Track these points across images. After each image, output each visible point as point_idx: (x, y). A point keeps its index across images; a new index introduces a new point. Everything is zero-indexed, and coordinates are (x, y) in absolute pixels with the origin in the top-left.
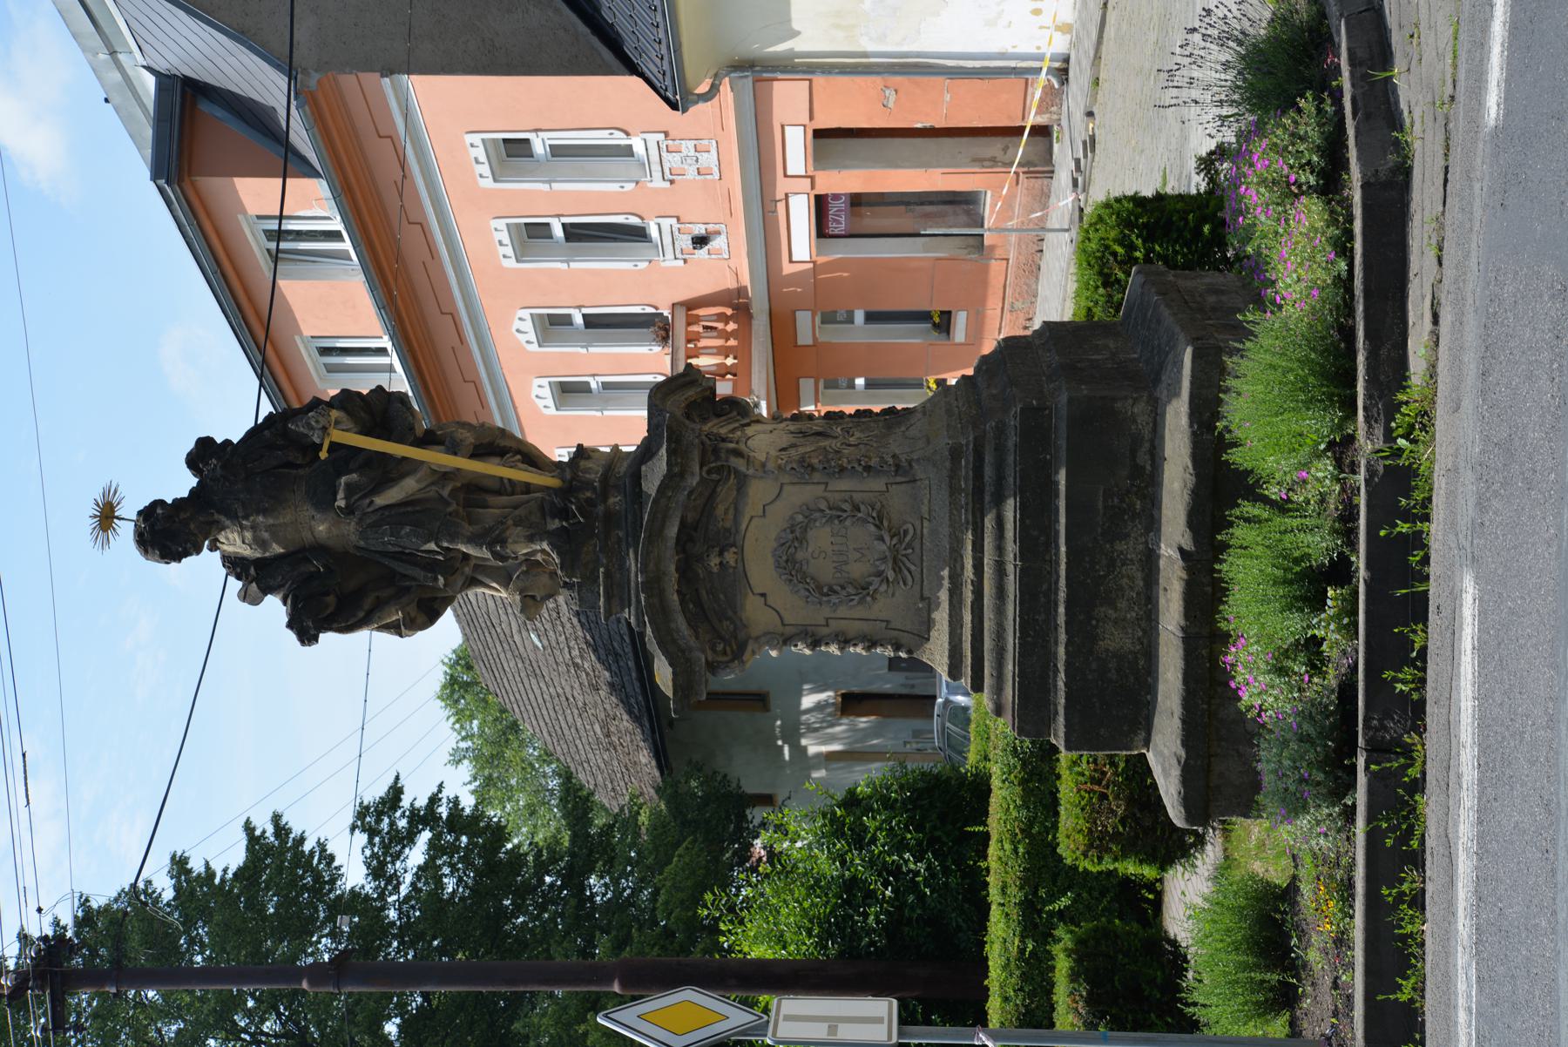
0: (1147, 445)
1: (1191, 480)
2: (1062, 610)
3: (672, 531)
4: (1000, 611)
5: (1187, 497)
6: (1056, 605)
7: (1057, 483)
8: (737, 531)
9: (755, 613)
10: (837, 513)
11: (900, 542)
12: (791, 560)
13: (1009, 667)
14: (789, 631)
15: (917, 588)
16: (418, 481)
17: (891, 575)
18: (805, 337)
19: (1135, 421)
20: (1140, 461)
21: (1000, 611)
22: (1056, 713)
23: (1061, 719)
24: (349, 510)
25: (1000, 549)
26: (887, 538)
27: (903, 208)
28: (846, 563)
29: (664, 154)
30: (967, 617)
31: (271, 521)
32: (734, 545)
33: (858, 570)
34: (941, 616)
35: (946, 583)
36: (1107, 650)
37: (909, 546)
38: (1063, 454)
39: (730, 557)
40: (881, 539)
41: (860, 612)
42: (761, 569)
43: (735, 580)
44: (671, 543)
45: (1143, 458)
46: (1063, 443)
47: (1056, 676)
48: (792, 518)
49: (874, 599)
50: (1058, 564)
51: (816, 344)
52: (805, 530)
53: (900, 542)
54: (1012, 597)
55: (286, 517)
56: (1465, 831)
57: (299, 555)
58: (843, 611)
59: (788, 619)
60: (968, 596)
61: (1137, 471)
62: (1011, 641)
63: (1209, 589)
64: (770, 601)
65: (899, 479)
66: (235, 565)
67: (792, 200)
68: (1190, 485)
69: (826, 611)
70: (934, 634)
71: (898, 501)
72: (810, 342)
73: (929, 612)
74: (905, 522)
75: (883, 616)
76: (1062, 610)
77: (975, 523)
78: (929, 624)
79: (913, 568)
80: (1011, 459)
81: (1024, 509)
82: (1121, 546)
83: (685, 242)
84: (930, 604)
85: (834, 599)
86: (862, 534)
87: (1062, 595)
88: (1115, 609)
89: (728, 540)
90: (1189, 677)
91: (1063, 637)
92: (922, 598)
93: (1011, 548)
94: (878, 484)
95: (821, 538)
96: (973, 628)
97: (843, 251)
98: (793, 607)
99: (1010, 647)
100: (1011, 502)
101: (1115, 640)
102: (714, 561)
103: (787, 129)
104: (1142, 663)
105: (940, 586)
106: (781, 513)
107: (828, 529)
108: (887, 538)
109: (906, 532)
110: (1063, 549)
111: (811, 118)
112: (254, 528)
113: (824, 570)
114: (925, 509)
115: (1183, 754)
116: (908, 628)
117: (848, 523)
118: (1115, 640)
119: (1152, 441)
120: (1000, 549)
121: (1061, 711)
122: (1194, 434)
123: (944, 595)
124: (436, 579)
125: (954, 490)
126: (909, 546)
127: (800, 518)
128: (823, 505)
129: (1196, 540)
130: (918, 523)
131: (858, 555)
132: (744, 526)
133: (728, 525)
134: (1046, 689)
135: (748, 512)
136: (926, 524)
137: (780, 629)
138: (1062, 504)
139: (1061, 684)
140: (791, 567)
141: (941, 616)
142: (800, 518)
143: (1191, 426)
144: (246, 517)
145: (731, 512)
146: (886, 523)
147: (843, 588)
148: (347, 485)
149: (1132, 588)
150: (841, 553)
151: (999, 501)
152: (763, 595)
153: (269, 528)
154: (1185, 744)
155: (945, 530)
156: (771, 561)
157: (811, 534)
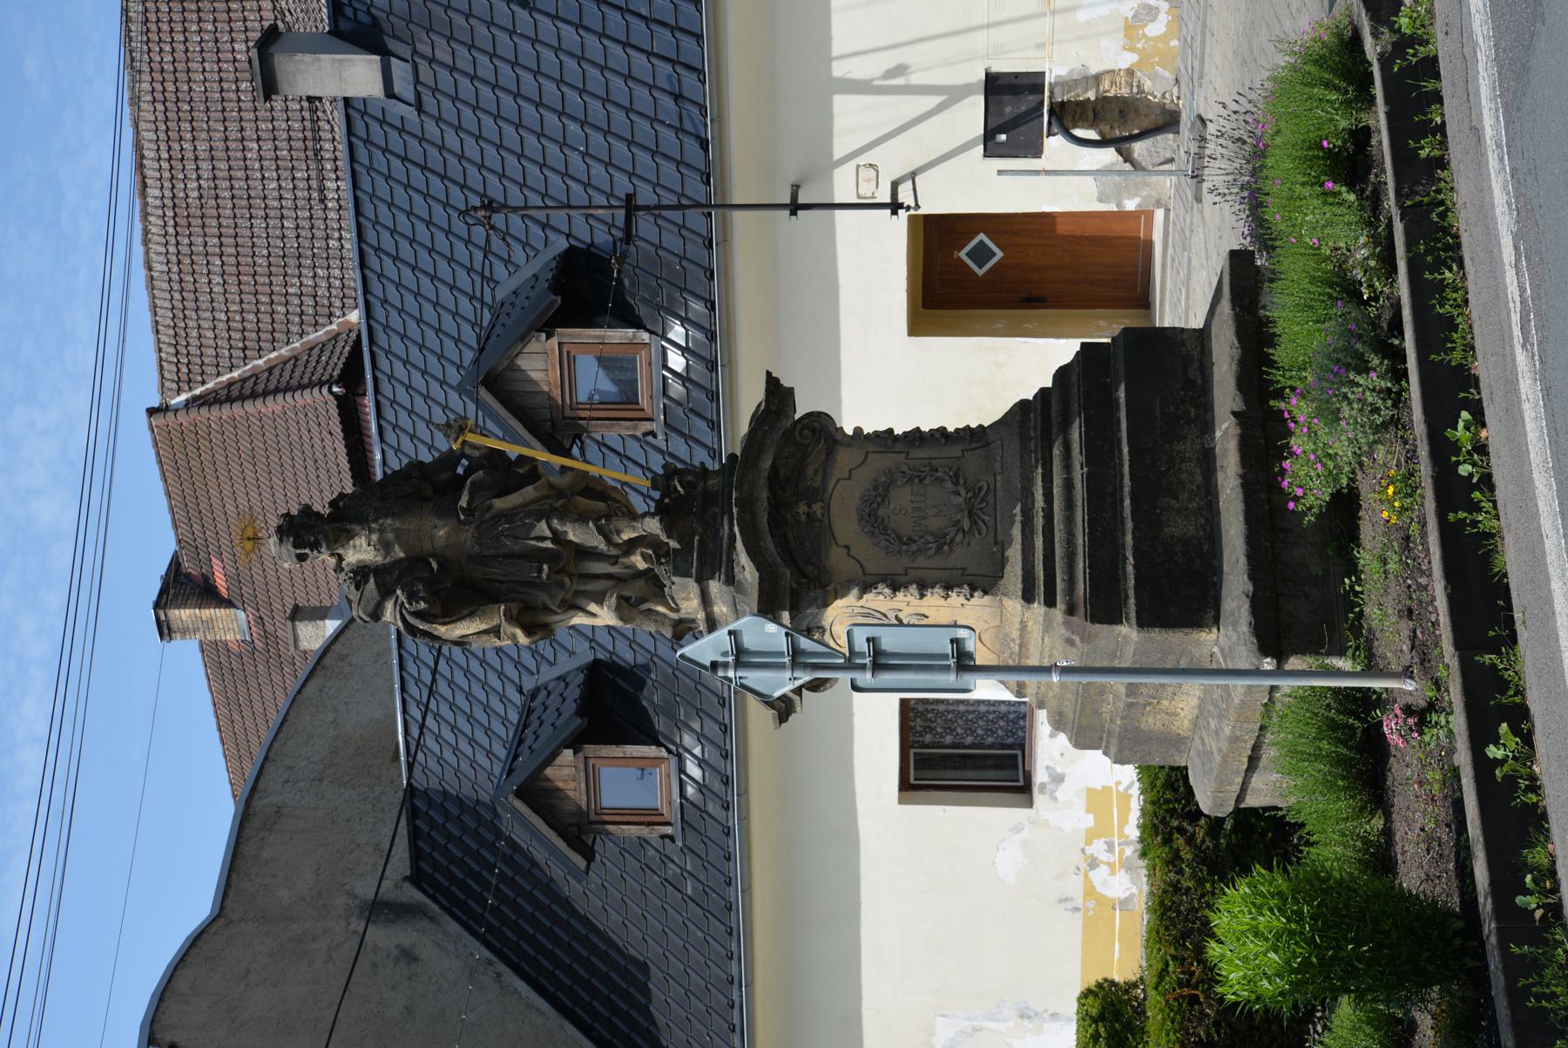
1: (1237, 353)
2: (1127, 502)
4: (1069, 520)
5: (1234, 367)
6: (1122, 501)
7: (1117, 399)
8: (825, 490)
9: (836, 559)
10: (916, 477)
11: (975, 496)
12: (873, 514)
13: (1080, 576)
14: (869, 579)
15: (991, 535)
17: (966, 525)
19: (1185, 345)
21: (1069, 520)
22: (1127, 597)
23: (1132, 601)
24: (469, 511)
25: (1068, 467)
26: (963, 492)
28: (925, 518)
30: (1039, 542)
31: (398, 525)
33: (935, 523)
34: (1015, 553)
35: (1019, 518)
36: (1172, 536)
37: (983, 500)
38: (1122, 373)
39: (817, 508)
40: (958, 493)
41: (936, 562)
42: (845, 523)
43: (820, 530)
44: (765, 474)
45: (1193, 373)
46: (1121, 365)
47: (1124, 563)
49: (951, 550)
50: (1121, 465)
52: (887, 488)
53: (975, 496)
54: (1079, 503)
55: (411, 524)
56: (1491, 123)
58: (921, 561)
59: (870, 569)
60: (1039, 522)
62: (1080, 540)
63: (1262, 442)
64: (853, 552)
65: (975, 445)
68: (1237, 357)
69: (906, 561)
70: (1008, 568)
73: (1003, 551)
76: (1127, 502)
77: (1043, 459)
78: (1002, 562)
80: (1075, 390)
81: (1088, 425)
84: (1003, 545)
85: (914, 547)
87: (1127, 489)
88: (1177, 500)
89: (816, 495)
90: (1250, 517)
91: (1129, 525)
92: (996, 543)
93: (1079, 474)
95: (902, 497)
96: (1045, 549)
98: (870, 553)
99: (1080, 549)
100: (1076, 424)
101: (1179, 527)
102: (802, 508)
104: (1206, 547)
105: (1013, 523)
106: (865, 477)
107: (908, 489)
108: (963, 492)
109: (980, 489)
110: (1126, 450)
112: (381, 530)
114: (998, 465)
117: (927, 481)
119: (1201, 360)
120: (1068, 467)
121: (1131, 593)
122: (1236, 315)
123: (1016, 532)
124: (540, 570)
126: (983, 500)
128: (904, 468)
129: (1246, 400)
130: (991, 480)
131: (935, 511)
133: (817, 484)
134: (1116, 578)
136: (999, 478)
138: (1123, 415)
139: (1130, 569)
140: (872, 516)
141: (1015, 553)
143: (1233, 308)
144: (376, 521)
145: (820, 474)
148: (473, 483)
149: (1192, 482)
150: (918, 509)
151: (1065, 427)
152: (847, 547)
153: (394, 530)
154: (1251, 577)
155: (1017, 472)
156: (855, 517)
157: (892, 494)
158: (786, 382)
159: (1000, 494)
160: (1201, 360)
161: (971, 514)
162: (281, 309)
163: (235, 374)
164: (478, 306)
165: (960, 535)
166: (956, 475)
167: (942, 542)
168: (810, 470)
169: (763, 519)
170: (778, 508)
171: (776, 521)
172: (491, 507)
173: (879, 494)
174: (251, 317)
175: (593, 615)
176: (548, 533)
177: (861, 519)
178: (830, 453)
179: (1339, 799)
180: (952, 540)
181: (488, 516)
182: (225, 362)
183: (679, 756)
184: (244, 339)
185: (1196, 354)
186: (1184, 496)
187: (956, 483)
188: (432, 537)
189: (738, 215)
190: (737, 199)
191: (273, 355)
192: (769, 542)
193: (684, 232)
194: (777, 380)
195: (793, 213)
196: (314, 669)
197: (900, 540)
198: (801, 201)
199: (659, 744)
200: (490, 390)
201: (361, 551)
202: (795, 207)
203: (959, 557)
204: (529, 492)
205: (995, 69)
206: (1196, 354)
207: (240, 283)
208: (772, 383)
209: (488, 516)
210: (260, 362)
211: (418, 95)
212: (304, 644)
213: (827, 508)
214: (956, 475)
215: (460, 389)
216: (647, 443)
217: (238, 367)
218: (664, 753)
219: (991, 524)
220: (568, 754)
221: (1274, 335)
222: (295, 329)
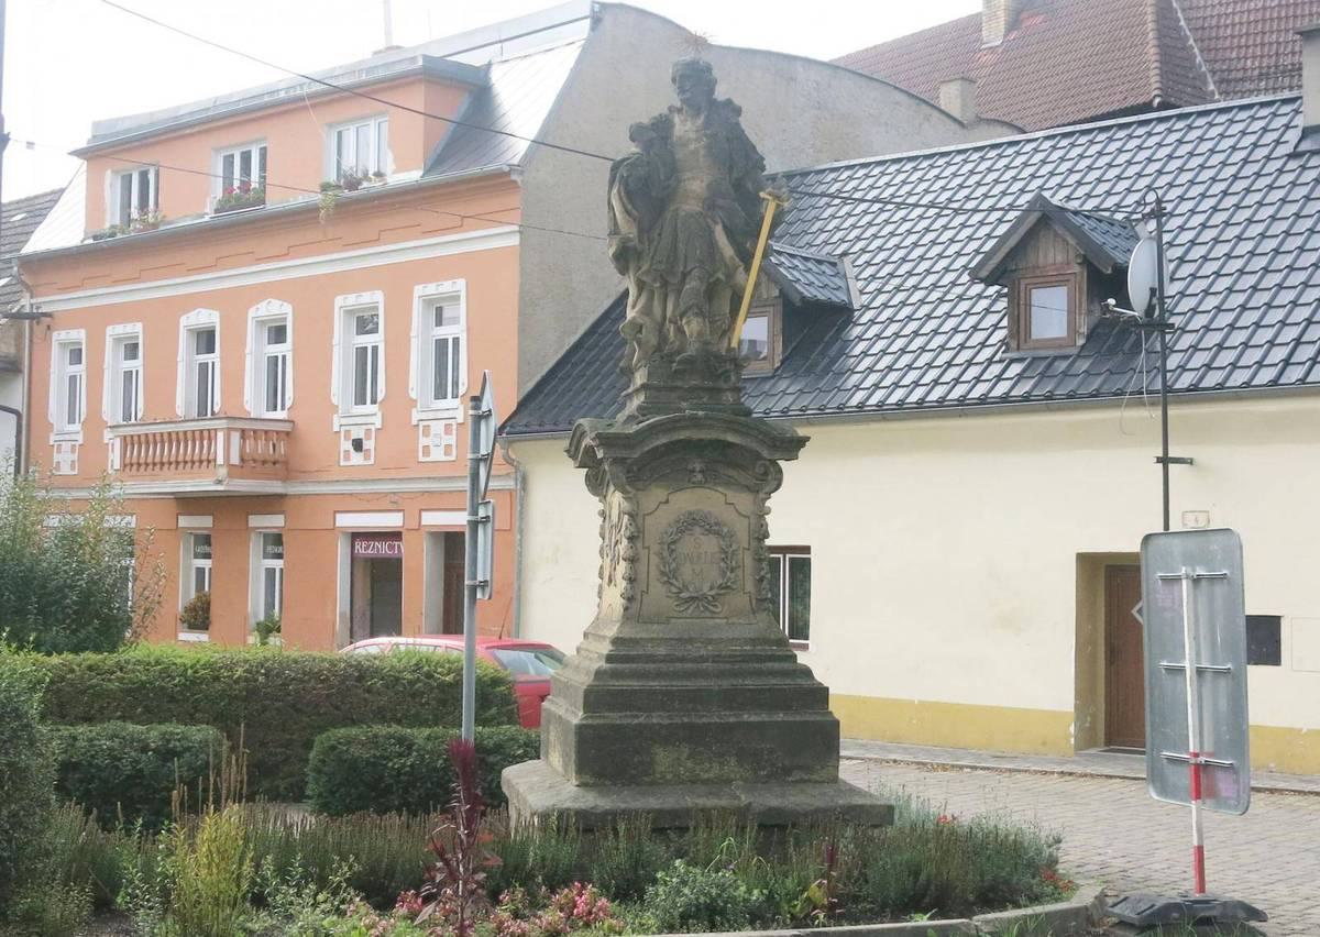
0: (806, 778)
3: (731, 438)
8: (715, 484)
9: (657, 494)
10: (726, 555)
11: (709, 602)
16: (732, 258)
17: (685, 595)
18: (256, 521)
20: (795, 772)
26: (713, 593)
27: (369, 597)
28: (692, 563)
29: (444, 422)
32: (706, 479)
33: (686, 572)
37: (707, 608)
39: (700, 477)
40: (711, 589)
41: (654, 573)
42: (687, 501)
46: (791, 719)
48: (725, 525)
49: (665, 583)
51: (248, 529)
52: (717, 533)
57: (674, 169)
58: (654, 560)
59: (649, 520)
61: (787, 771)
64: (663, 507)
65: (754, 602)
66: (662, 126)
67: (400, 515)
69: (655, 548)
71: (739, 600)
72: (250, 525)
74: (723, 605)
75: (651, 589)
79: (689, 611)
82: (733, 761)
83: (357, 433)
85: (666, 554)
86: (713, 576)
89: (711, 477)
94: (750, 586)
95: (710, 545)
97: (342, 551)
101: (663, 758)
103: (401, 514)
104: (646, 779)
106: (728, 515)
107: (717, 549)
109: (715, 606)
111: (408, 530)
113: (686, 546)
114: (735, 620)
115: (598, 811)
116: (644, 608)
117: (722, 564)
118: (663, 758)
125: (753, 641)
127: (725, 530)
128: (734, 547)
132: (720, 489)
135: (730, 493)
137: (641, 514)
140: (690, 522)
142: (725, 530)
146: (723, 591)
147: (674, 560)
152: (667, 502)
158: (802, 453)
159: (711, 622)
160: (809, 781)
161: (692, 599)
162: (1234, 55)
163: (1182, 23)
164: (1129, 210)
165: (674, 590)
166: (728, 587)
167: (669, 576)
168: (731, 472)
169: (682, 435)
170: (697, 447)
171: (687, 445)
172: (716, 223)
173: (713, 528)
174: (1229, 32)
175: (634, 307)
176: (689, 268)
177: (690, 514)
178: (748, 489)
179: (937, 890)
180: (671, 584)
181: (709, 221)
182: (1193, 14)
183: (773, 377)
184: (1211, 28)
185: (815, 777)
186: (689, 764)
187: (720, 587)
188: (693, 179)
189: (1157, 413)
190: (1172, 411)
191: (1196, 50)
192: (663, 440)
193: (1179, 370)
194: (803, 446)
195: (1159, 460)
196: (917, 98)
197: (674, 542)
198: (1171, 466)
199: (783, 362)
200: (1039, 221)
201: (683, 127)
202: (1165, 461)
203: (658, 590)
204: (727, 249)
205: (1283, 621)
206: (815, 777)
207: (1257, 22)
208: (808, 439)
209: (709, 221)
210: (1191, 42)
211: (1301, 154)
212: (944, 89)
213: (700, 485)
214: (728, 587)
215: (1039, 197)
216: (1001, 347)
217: (1188, 25)
218: (777, 365)
219: (685, 614)
220: (776, 293)
221: (1015, 841)
222: (1217, 66)
